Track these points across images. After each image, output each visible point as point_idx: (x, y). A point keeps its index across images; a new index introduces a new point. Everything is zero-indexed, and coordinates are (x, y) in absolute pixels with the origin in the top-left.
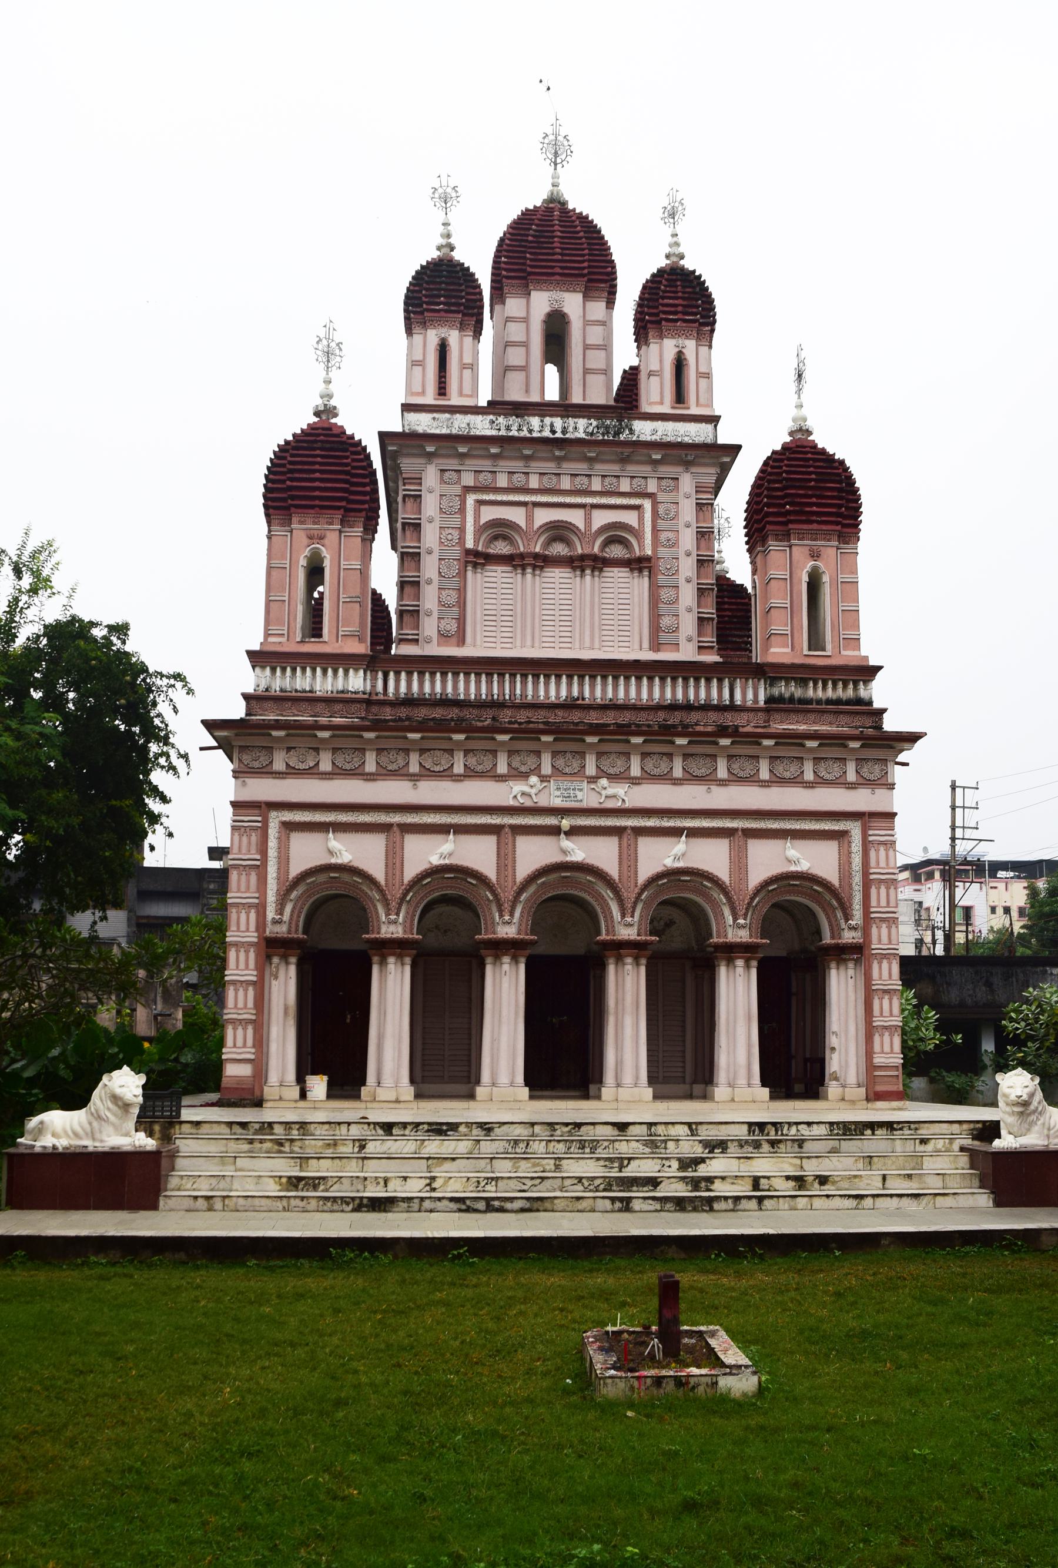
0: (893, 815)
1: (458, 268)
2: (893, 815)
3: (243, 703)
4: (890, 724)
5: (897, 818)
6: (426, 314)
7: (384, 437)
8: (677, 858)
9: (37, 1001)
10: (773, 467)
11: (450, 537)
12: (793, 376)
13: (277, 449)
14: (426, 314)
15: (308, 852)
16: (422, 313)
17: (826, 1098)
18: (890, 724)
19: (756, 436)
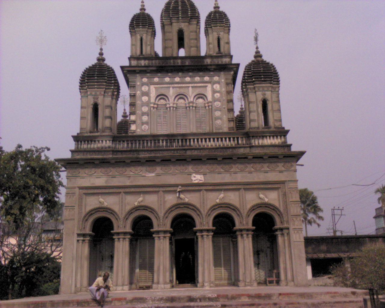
0: (297, 181)
1: (223, 14)
2: (297, 181)
3: (70, 153)
4: (294, 149)
5: (298, 182)
6: (136, 29)
7: (122, 68)
8: (221, 200)
9: (15, 278)
10: (248, 67)
11: (145, 99)
12: (259, 38)
13: (82, 74)
14: (136, 29)
15: (92, 203)
16: (134, 29)
17: (280, 286)
18: (294, 149)
19: (242, 57)
